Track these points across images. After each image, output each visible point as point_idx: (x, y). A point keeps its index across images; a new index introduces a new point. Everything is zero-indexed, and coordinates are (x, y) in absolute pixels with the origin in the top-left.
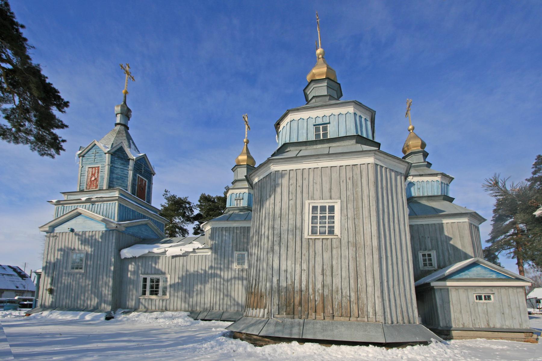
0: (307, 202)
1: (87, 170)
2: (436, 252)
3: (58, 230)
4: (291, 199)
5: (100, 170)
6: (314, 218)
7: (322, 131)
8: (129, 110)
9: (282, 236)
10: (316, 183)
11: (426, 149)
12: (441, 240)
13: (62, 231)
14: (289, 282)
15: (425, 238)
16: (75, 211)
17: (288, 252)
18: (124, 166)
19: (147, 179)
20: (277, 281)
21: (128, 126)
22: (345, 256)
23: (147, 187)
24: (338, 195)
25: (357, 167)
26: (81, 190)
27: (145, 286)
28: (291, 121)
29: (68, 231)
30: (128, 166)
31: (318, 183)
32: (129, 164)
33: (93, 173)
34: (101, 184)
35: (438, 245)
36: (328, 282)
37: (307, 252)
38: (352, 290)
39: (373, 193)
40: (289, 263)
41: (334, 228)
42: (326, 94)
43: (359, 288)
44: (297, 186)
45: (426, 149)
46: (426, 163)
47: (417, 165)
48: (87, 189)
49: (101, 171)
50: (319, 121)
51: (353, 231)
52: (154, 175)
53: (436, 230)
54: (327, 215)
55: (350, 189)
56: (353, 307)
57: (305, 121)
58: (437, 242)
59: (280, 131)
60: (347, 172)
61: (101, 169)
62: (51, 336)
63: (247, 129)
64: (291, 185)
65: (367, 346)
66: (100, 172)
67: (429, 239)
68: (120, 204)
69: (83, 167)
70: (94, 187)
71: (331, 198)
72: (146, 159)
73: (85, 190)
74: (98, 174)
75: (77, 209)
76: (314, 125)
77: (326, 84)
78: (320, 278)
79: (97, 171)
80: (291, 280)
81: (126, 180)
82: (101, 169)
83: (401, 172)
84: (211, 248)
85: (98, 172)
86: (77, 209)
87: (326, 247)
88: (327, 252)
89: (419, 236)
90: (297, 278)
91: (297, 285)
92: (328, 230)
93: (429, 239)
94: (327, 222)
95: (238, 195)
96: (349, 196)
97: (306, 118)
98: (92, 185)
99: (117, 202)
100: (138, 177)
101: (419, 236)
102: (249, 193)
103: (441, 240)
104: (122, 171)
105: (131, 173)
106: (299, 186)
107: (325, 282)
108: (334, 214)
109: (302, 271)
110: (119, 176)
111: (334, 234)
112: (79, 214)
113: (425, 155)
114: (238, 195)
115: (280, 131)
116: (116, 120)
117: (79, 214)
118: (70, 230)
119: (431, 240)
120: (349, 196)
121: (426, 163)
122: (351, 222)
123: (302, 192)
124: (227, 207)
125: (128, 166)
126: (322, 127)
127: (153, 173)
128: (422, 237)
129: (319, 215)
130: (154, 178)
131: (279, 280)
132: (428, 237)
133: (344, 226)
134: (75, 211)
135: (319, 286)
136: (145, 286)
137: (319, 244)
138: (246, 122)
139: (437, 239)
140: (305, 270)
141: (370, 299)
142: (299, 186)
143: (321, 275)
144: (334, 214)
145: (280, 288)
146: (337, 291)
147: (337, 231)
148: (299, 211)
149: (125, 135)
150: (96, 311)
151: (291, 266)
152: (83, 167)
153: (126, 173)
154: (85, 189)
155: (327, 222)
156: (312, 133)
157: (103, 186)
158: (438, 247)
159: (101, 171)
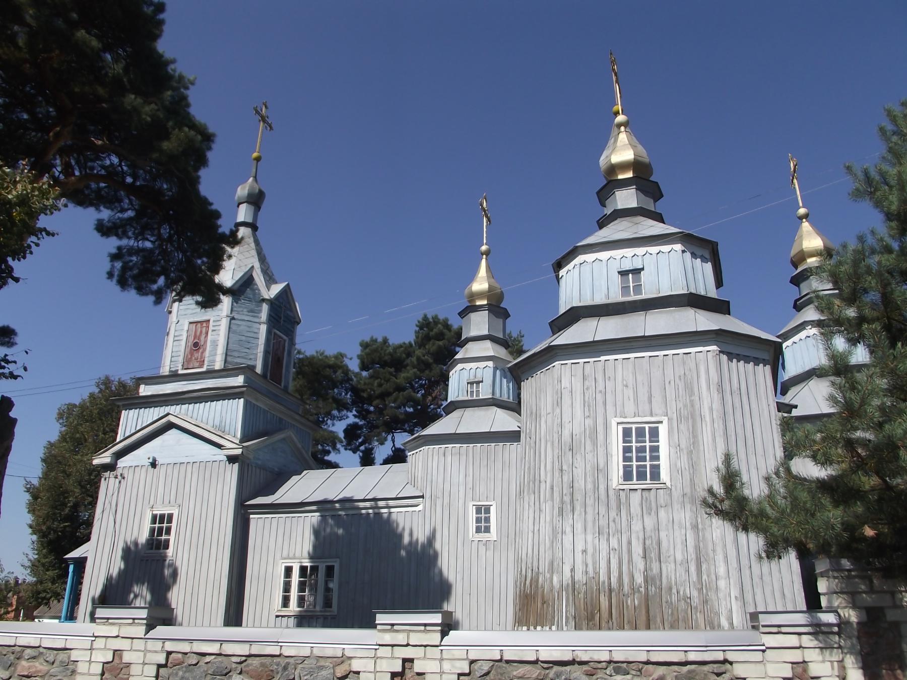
0: (614, 422)
1: (186, 328)
4: (589, 416)
5: (211, 328)
6: (627, 450)
7: (633, 283)
9: (576, 485)
10: (627, 386)
13: (134, 464)
14: (591, 574)
16: (164, 420)
17: (587, 516)
20: (571, 572)
21: (257, 225)
22: (680, 523)
23: (286, 353)
25: (690, 357)
28: (581, 264)
29: (147, 462)
31: (630, 385)
33: (198, 333)
34: (211, 358)
36: (654, 571)
37: (617, 515)
38: (694, 585)
39: (717, 405)
40: (590, 538)
41: (659, 469)
43: (706, 581)
44: (597, 392)
49: (213, 331)
51: (690, 474)
54: (648, 444)
55: (682, 397)
56: (697, 617)
57: (604, 262)
59: (562, 276)
60: (676, 365)
61: (214, 326)
63: (487, 222)
64: (587, 389)
65: (216, 305)
66: (210, 333)
69: (178, 321)
70: (197, 364)
72: (289, 295)
73: (180, 372)
74: (205, 337)
78: (640, 564)
79: (204, 330)
80: (595, 568)
82: (214, 326)
83: (764, 358)
85: (207, 333)
90: (603, 565)
91: (603, 577)
94: (648, 458)
96: (681, 408)
100: (275, 334)
104: (249, 327)
105: (263, 328)
107: (649, 572)
108: (658, 442)
109: (611, 552)
110: (244, 338)
111: (660, 480)
112: (170, 426)
115: (562, 276)
116: (236, 217)
120: (681, 408)
122: (686, 457)
123: (605, 403)
124: (452, 396)
125: (259, 315)
126: (649, 427)
127: (298, 320)
129: (634, 445)
130: (299, 329)
131: (573, 570)
133: (676, 465)
134: (164, 420)
135: (639, 579)
137: (636, 498)
138: (485, 211)
140: (616, 550)
141: (724, 603)
143: (643, 558)
144: (658, 442)
145: (577, 586)
146: (670, 589)
147: (664, 475)
148: (601, 437)
149: (253, 245)
151: (593, 541)
152: (178, 321)
153: (256, 331)
154: (180, 367)
155: (648, 458)
157: (214, 361)
159: (213, 331)
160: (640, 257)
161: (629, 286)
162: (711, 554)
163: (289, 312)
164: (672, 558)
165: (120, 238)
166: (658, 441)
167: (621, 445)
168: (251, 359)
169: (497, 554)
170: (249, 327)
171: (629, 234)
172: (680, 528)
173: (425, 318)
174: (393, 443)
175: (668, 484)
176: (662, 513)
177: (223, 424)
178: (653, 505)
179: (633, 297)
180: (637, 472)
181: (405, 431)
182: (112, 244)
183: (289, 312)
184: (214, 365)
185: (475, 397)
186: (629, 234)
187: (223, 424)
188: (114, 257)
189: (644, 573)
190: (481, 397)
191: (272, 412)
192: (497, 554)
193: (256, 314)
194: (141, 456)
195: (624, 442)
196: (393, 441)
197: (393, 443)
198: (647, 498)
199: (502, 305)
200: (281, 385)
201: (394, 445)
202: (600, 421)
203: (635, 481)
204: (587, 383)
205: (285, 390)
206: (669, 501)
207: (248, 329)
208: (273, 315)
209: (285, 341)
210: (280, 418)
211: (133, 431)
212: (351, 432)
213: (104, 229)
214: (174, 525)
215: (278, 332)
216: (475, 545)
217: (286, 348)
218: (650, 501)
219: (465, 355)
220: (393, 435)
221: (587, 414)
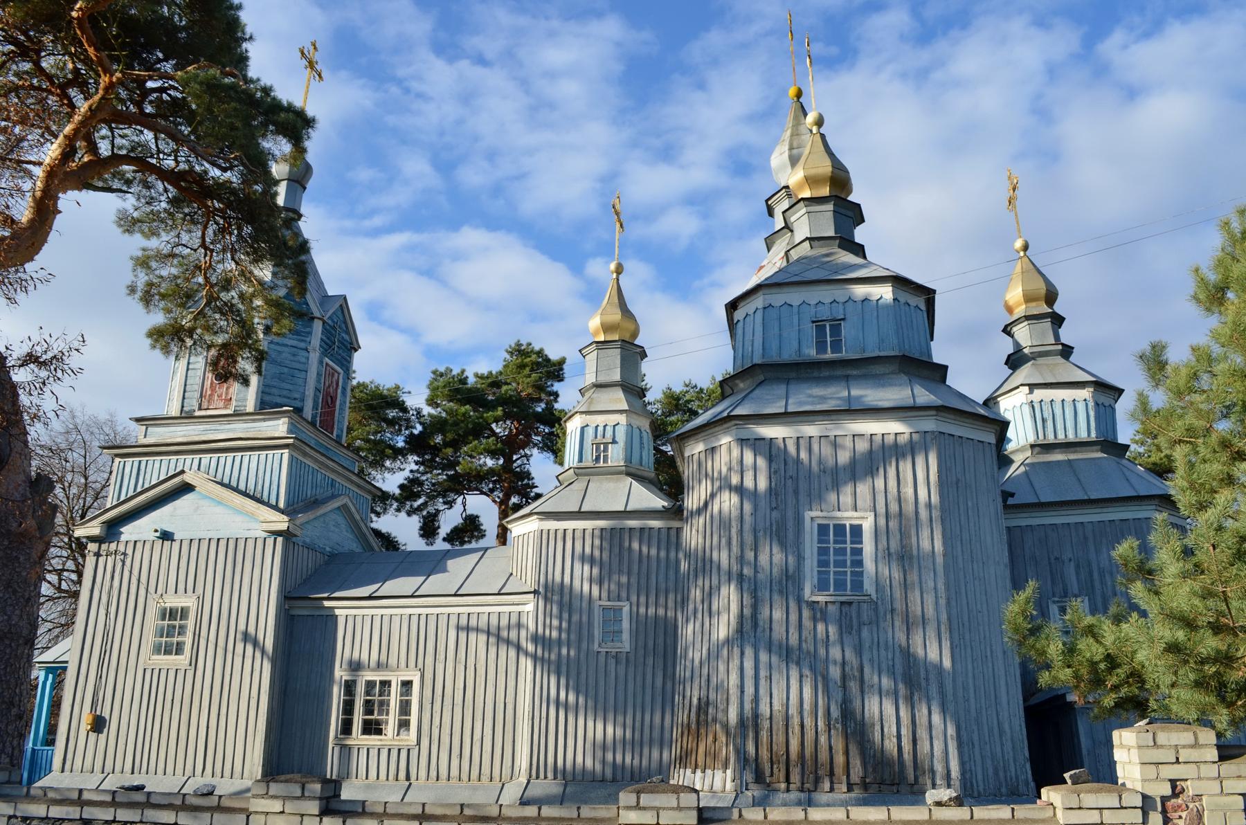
2: (1089, 600)
3: (129, 532)
8: (308, 169)
11: (1058, 308)
12: (1099, 565)
15: (1063, 562)
16: (177, 480)
18: (299, 340)
19: (342, 366)
23: (339, 391)
24: (869, 502)
26: (186, 412)
27: (405, 708)
29: (152, 536)
30: (308, 339)
32: (310, 333)
35: (1092, 581)
41: (863, 577)
42: (831, 233)
45: (1058, 308)
46: (1060, 347)
47: (1040, 352)
48: (200, 409)
50: (825, 313)
52: (356, 350)
53: (1086, 538)
57: (795, 310)
58: (1091, 574)
62: (751, 735)
67: (1072, 563)
68: (292, 456)
71: (856, 509)
72: (346, 310)
73: (197, 413)
75: (182, 472)
76: (813, 322)
77: (832, 206)
81: (300, 382)
84: (535, 592)
86: (182, 472)
87: (848, 623)
88: (850, 634)
89: (1049, 559)
92: (851, 581)
93: (1072, 563)
94: (849, 563)
95: (600, 429)
97: (796, 303)
98: (216, 398)
99: (287, 451)
100: (327, 364)
101: (1049, 559)
102: (629, 425)
103: (1099, 565)
104: (294, 355)
105: (314, 356)
106: (791, 477)
110: (286, 370)
113: (1058, 320)
114: (600, 429)
115: (738, 321)
117: (187, 488)
118: (158, 534)
119: (1078, 567)
121: (1060, 347)
128: (1056, 559)
132: (1070, 560)
134: (177, 480)
136: (405, 708)
139: (1090, 565)
142: (791, 477)
150: (283, 777)
153: (303, 360)
155: (849, 563)
156: (810, 340)
158: (1093, 586)
160: (841, 305)
161: (826, 341)
162: (923, 683)
163: (344, 335)
164: (876, 687)
165: (147, 237)
166: (861, 542)
167: (816, 545)
168: (295, 399)
169: (631, 670)
170: (294, 355)
171: (827, 273)
172: (887, 649)
173: (519, 344)
174: (464, 507)
175: (874, 596)
176: (865, 633)
177: (260, 487)
178: (855, 621)
179: (829, 355)
180: (835, 581)
181: (482, 493)
182: (137, 243)
183: (344, 335)
184: (246, 406)
185: (601, 464)
186: (827, 273)
187: (260, 487)
188: (143, 262)
189: (841, 706)
190: (610, 464)
191: (324, 472)
192: (631, 670)
193: (303, 338)
194: (140, 530)
195: (820, 541)
196: (464, 504)
197: (464, 507)
198: (846, 614)
199: (636, 342)
200: (332, 434)
201: (465, 510)
202: (790, 514)
203: (831, 592)
204: (774, 465)
205: (338, 442)
206: (874, 618)
207: (292, 358)
208: (324, 338)
209: (339, 374)
210: (333, 480)
211: (131, 493)
212: (409, 491)
213: (129, 224)
214: (190, 623)
215: (331, 363)
216: (602, 659)
217: (340, 384)
218: (851, 617)
219: (589, 407)
220: (464, 498)
221: (774, 505)
